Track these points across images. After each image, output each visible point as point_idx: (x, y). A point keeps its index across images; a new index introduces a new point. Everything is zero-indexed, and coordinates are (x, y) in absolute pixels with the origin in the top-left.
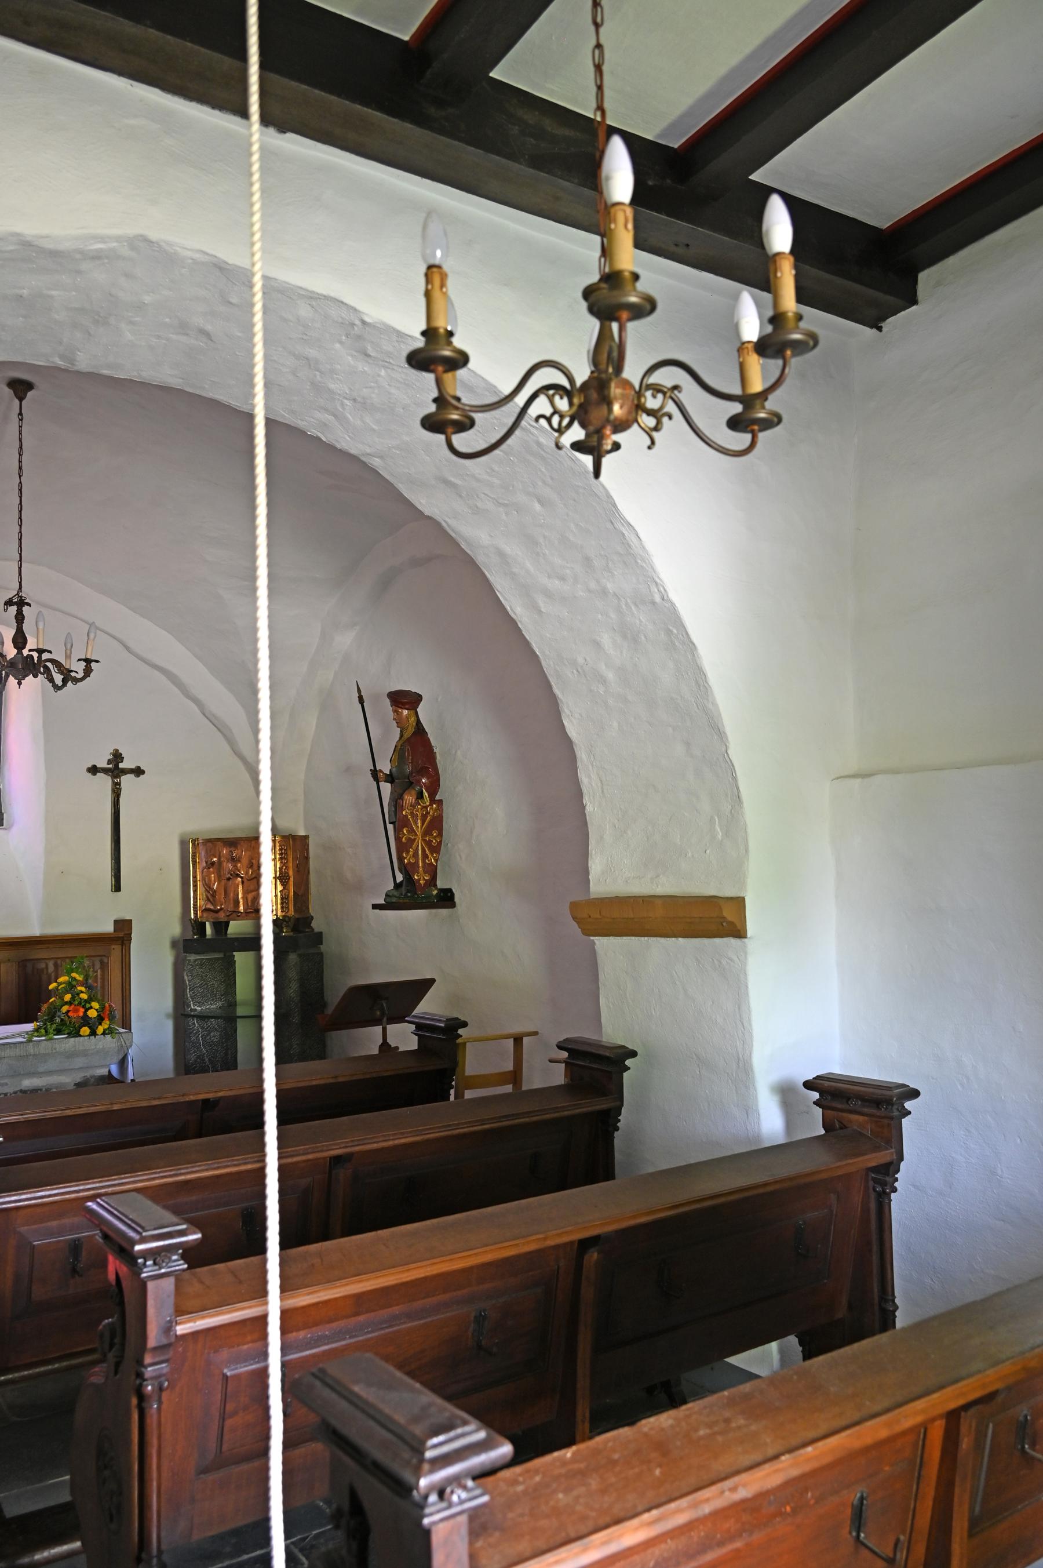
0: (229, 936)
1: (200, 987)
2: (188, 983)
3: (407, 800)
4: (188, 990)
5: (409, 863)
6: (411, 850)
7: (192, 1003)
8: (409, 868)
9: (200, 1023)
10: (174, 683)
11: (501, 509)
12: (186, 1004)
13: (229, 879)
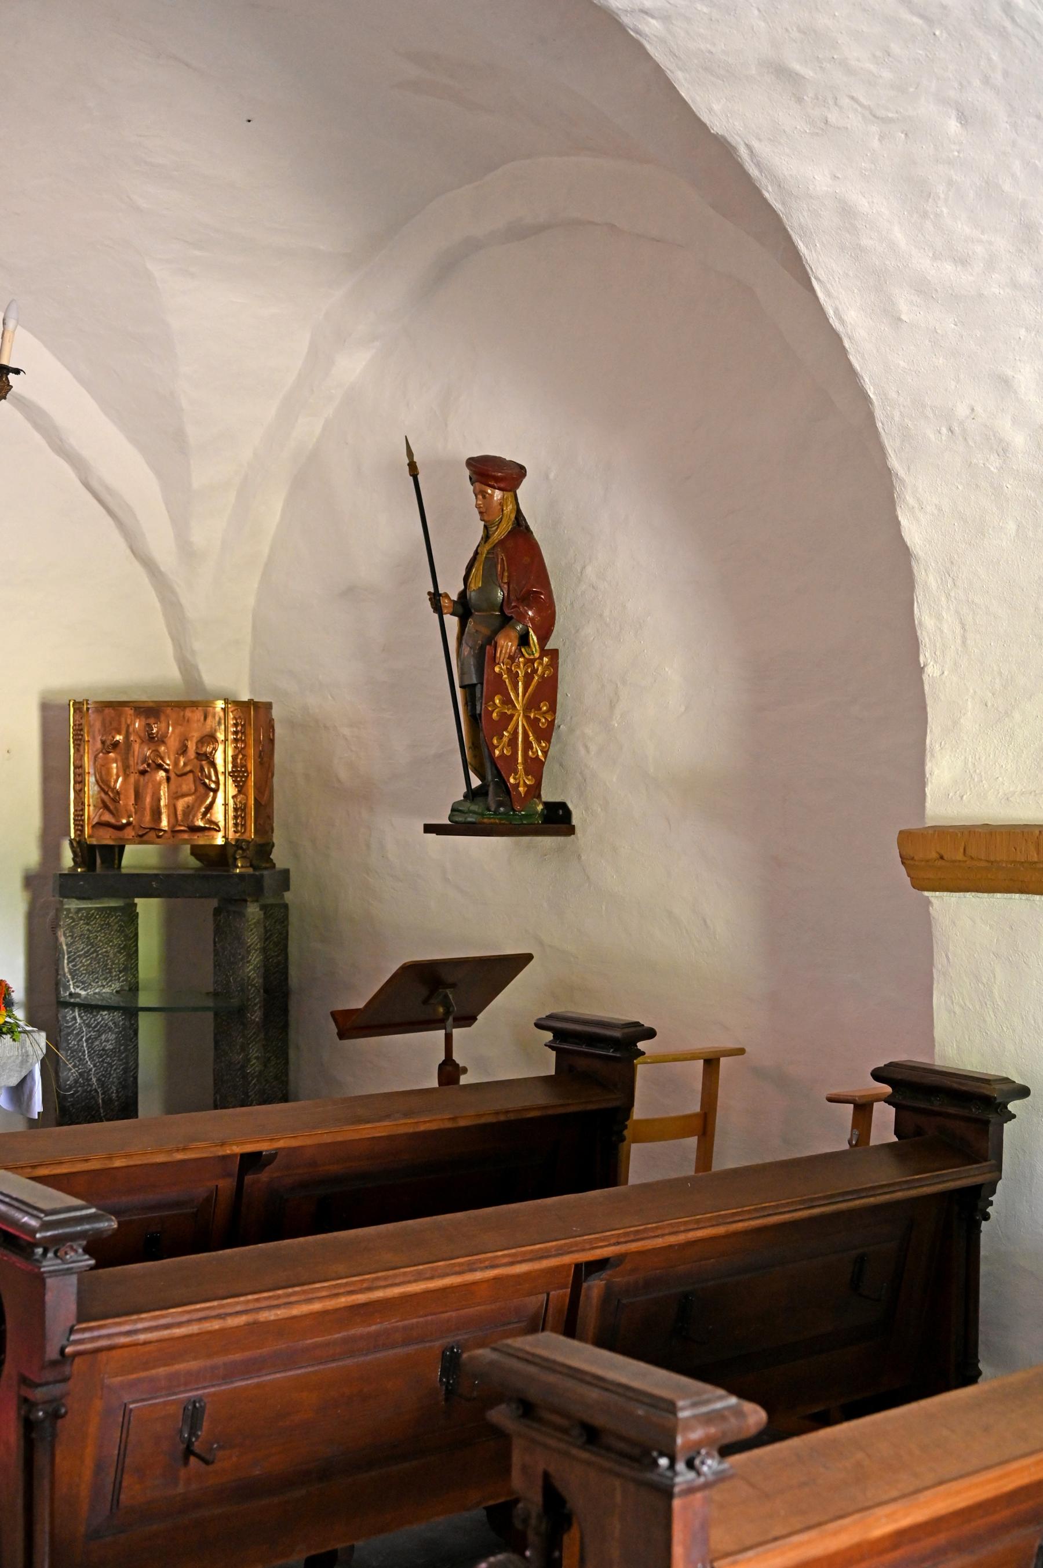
0: (124, 871)
1: (85, 955)
2: (65, 948)
3: (502, 647)
4: (66, 961)
5: (502, 755)
6: (505, 733)
7: (71, 982)
8: (500, 764)
9: (85, 1018)
10: (37, 426)
11: (874, 129)
12: (58, 984)
13: (143, 773)
